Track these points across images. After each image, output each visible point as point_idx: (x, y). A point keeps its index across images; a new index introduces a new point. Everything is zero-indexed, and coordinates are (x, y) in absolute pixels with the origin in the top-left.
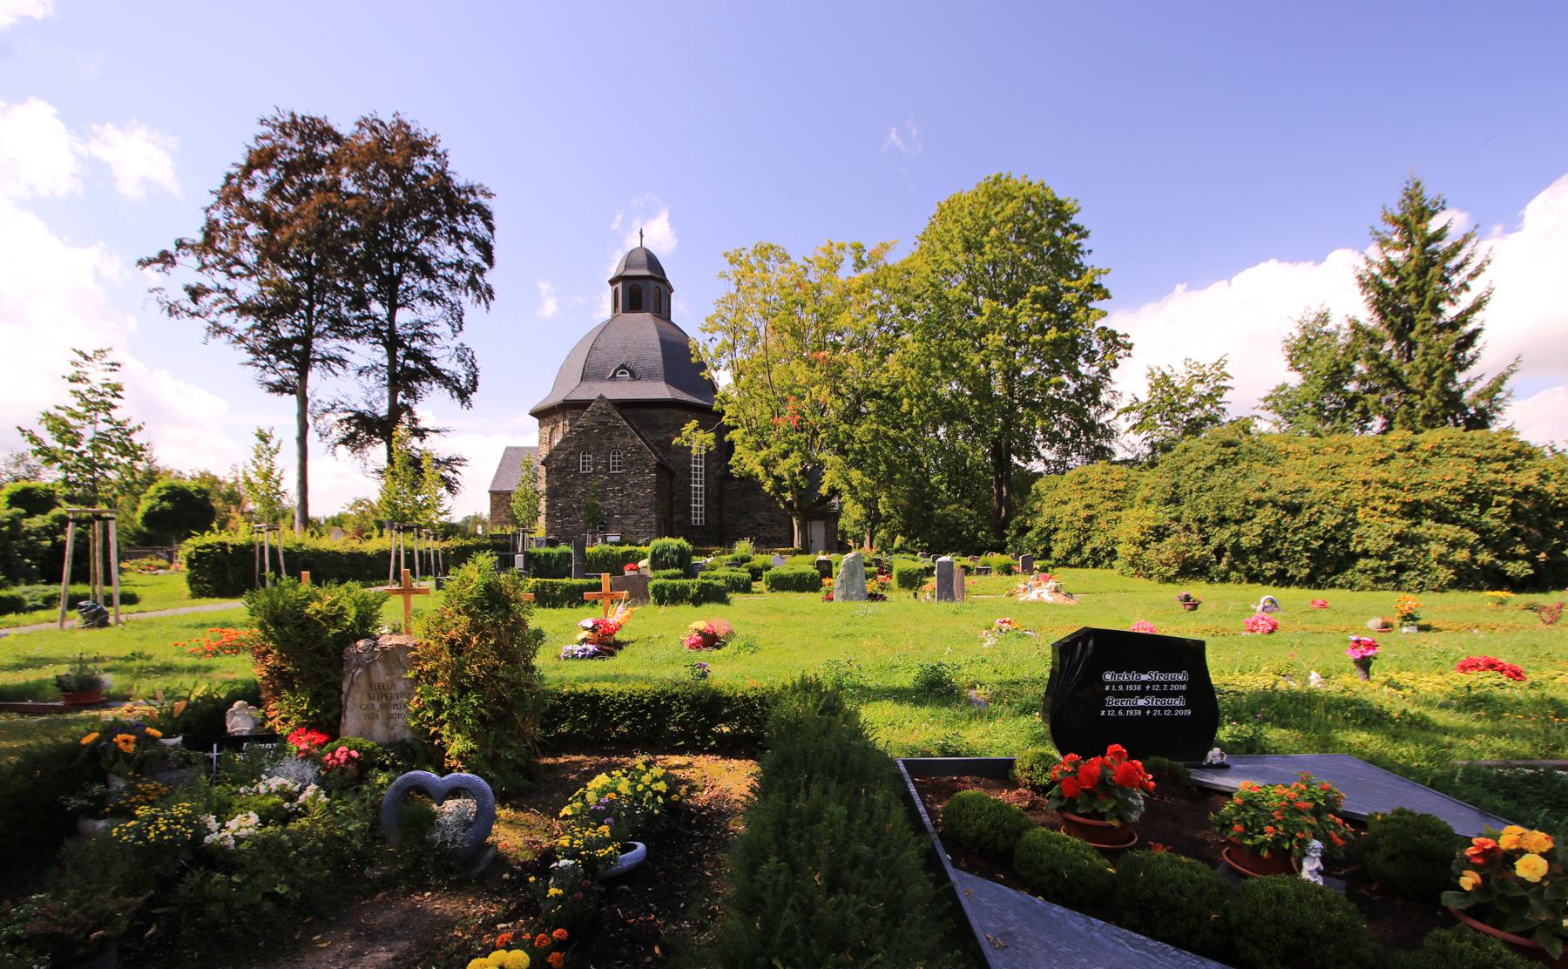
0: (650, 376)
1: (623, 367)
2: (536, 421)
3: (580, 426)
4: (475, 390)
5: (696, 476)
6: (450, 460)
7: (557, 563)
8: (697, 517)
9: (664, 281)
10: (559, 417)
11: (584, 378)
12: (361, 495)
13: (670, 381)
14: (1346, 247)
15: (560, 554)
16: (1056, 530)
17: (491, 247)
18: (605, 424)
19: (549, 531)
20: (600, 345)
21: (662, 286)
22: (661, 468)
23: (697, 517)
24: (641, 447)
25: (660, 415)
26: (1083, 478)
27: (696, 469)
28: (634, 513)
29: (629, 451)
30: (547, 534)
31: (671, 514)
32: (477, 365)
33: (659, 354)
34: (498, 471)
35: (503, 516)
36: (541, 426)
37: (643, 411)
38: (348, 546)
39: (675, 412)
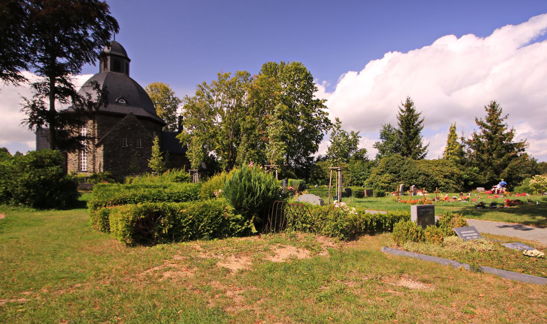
3: (121, 125)
9: (129, 60)
21: (127, 62)
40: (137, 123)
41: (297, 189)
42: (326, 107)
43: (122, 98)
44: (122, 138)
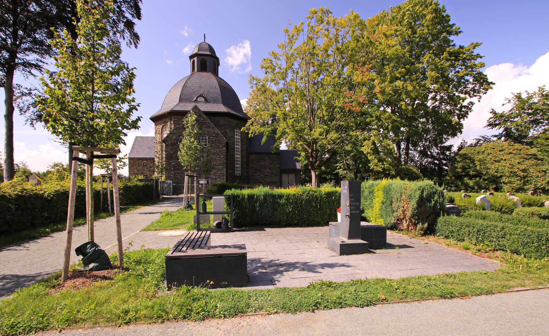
0: (215, 101)
1: (201, 96)
2: (153, 124)
8: (238, 172)
9: (217, 59)
11: (181, 100)
12: (57, 161)
13: (225, 104)
14: (506, 62)
16: (501, 176)
20: (189, 85)
21: (215, 60)
22: (227, 145)
23: (238, 172)
24: (217, 134)
25: (222, 121)
26: (501, 149)
29: (211, 136)
33: (219, 90)
34: (133, 147)
35: (136, 171)
36: (156, 125)
38: (19, 188)
39: (229, 119)
40: (203, 117)
41: (409, 214)
42: (478, 56)
43: (201, 96)
44: (203, 137)
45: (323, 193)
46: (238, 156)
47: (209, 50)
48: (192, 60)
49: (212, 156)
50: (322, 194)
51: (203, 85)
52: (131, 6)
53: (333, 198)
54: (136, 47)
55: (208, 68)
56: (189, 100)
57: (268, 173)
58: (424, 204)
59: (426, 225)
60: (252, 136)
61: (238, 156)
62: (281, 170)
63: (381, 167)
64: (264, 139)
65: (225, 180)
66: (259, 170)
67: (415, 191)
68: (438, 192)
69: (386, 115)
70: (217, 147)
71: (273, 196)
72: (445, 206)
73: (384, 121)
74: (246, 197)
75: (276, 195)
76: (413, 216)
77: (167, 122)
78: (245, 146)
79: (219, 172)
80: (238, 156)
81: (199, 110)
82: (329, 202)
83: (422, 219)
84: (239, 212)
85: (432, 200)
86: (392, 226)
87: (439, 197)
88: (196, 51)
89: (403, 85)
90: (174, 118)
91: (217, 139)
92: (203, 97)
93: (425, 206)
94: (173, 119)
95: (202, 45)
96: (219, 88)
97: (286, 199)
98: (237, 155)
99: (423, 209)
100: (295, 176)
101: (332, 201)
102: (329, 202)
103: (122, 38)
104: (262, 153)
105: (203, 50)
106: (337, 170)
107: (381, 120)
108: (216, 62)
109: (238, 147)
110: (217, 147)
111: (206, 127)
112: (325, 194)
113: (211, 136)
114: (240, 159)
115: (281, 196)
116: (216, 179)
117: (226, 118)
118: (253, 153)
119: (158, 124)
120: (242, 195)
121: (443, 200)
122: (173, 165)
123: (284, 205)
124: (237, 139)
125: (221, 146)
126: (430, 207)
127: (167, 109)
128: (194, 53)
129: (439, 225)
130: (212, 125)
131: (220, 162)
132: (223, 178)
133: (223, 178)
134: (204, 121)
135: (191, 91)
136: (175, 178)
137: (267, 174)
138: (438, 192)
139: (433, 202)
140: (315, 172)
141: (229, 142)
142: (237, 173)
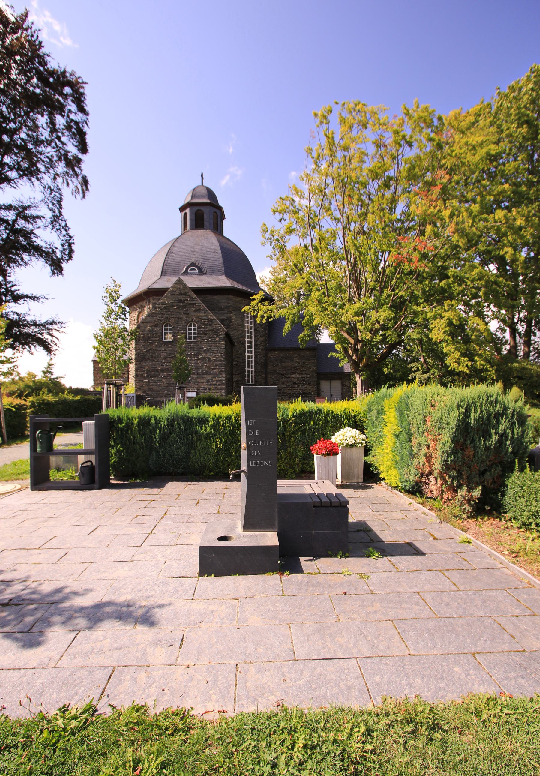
0: (214, 271)
1: (193, 264)
3: (162, 304)
4: (70, 258)
5: (248, 347)
6: (47, 323)
7: (164, 438)
9: (220, 209)
10: (144, 303)
11: (164, 273)
13: (228, 275)
15: (172, 420)
17: (85, 134)
18: (183, 302)
19: (138, 389)
21: (218, 212)
22: (228, 337)
24: (212, 320)
25: (223, 300)
27: (248, 342)
28: (207, 373)
30: (136, 391)
31: (232, 374)
32: (71, 233)
33: (219, 255)
37: (209, 297)
39: (234, 298)
40: (190, 296)
41: (437, 464)
44: (190, 326)
45: (291, 414)
46: (250, 354)
47: (207, 197)
48: (183, 213)
49: (204, 355)
50: (287, 415)
51: (197, 249)
52: (74, 133)
53: (312, 423)
54: (84, 197)
55: (206, 224)
56: (175, 272)
57: (298, 379)
58: (473, 441)
59: (477, 493)
60: (264, 321)
61: (250, 354)
62: (318, 374)
63: (467, 366)
64: (287, 327)
65: (223, 391)
66: (283, 375)
67: (451, 409)
68: (510, 411)
69: (474, 273)
70: (211, 341)
71: (188, 420)
72: (527, 447)
73: (469, 283)
74: (136, 422)
75: (193, 417)
76: (447, 468)
77: (145, 307)
78: (261, 339)
79: (214, 379)
80: (250, 354)
81: (185, 285)
82: (303, 432)
83: (468, 477)
84: (123, 451)
85: (493, 432)
86: (413, 487)
87: (512, 425)
88: (188, 199)
89: (505, 216)
90: (153, 299)
91: (211, 328)
92: (197, 267)
93: (475, 447)
94: (152, 301)
95: (198, 190)
96: (220, 251)
97: (214, 426)
98: (248, 352)
99: (470, 452)
100: (342, 383)
101: (310, 429)
102: (303, 432)
103: (65, 184)
104: (288, 349)
105: (199, 197)
106: (413, 374)
107: (464, 282)
108: (219, 214)
109: (250, 340)
110: (211, 341)
111: (195, 311)
112: (293, 416)
113: (203, 323)
114: (253, 359)
115: (203, 421)
116: (210, 389)
117: (230, 296)
118: (275, 350)
119: (133, 310)
120: (128, 419)
121: (523, 432)
122: (147, 370)
123: (208, 436)
124: (248, 328)
125: (217, 339)
126: (487, 449)
127: (144, 287)
128: (186, 202)
129: (510, 492)
130: (204, 306)
131: (216, 363)
132: (221, 389)
133: (221, 389)
134: (191, 302)
135: (179, 259)
136: (150, 389)
137: (296, 381)
138: (510, 411)
139: (495, 438)
140: (361, 376)
141: (232, 333)
142: (249, 381)
